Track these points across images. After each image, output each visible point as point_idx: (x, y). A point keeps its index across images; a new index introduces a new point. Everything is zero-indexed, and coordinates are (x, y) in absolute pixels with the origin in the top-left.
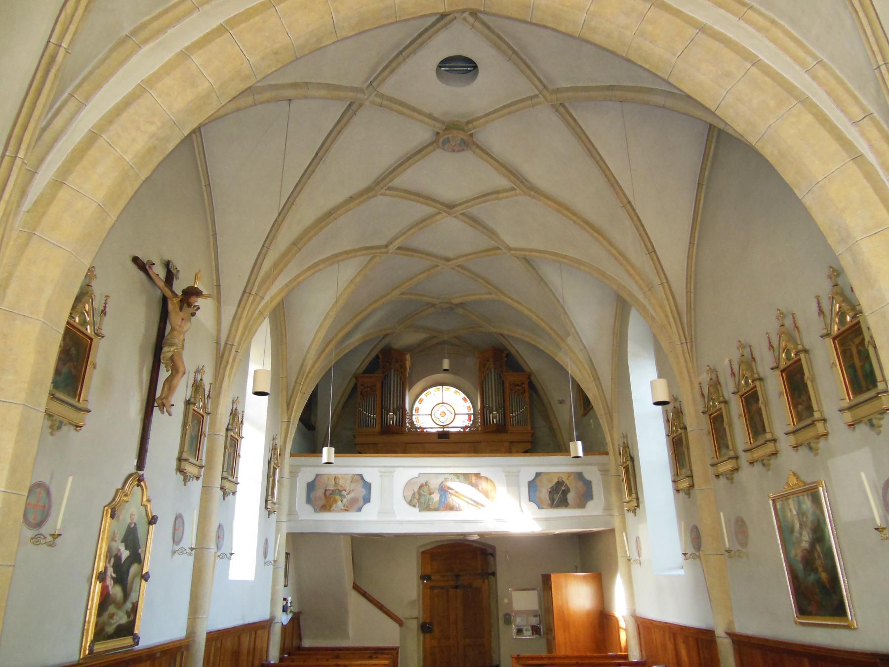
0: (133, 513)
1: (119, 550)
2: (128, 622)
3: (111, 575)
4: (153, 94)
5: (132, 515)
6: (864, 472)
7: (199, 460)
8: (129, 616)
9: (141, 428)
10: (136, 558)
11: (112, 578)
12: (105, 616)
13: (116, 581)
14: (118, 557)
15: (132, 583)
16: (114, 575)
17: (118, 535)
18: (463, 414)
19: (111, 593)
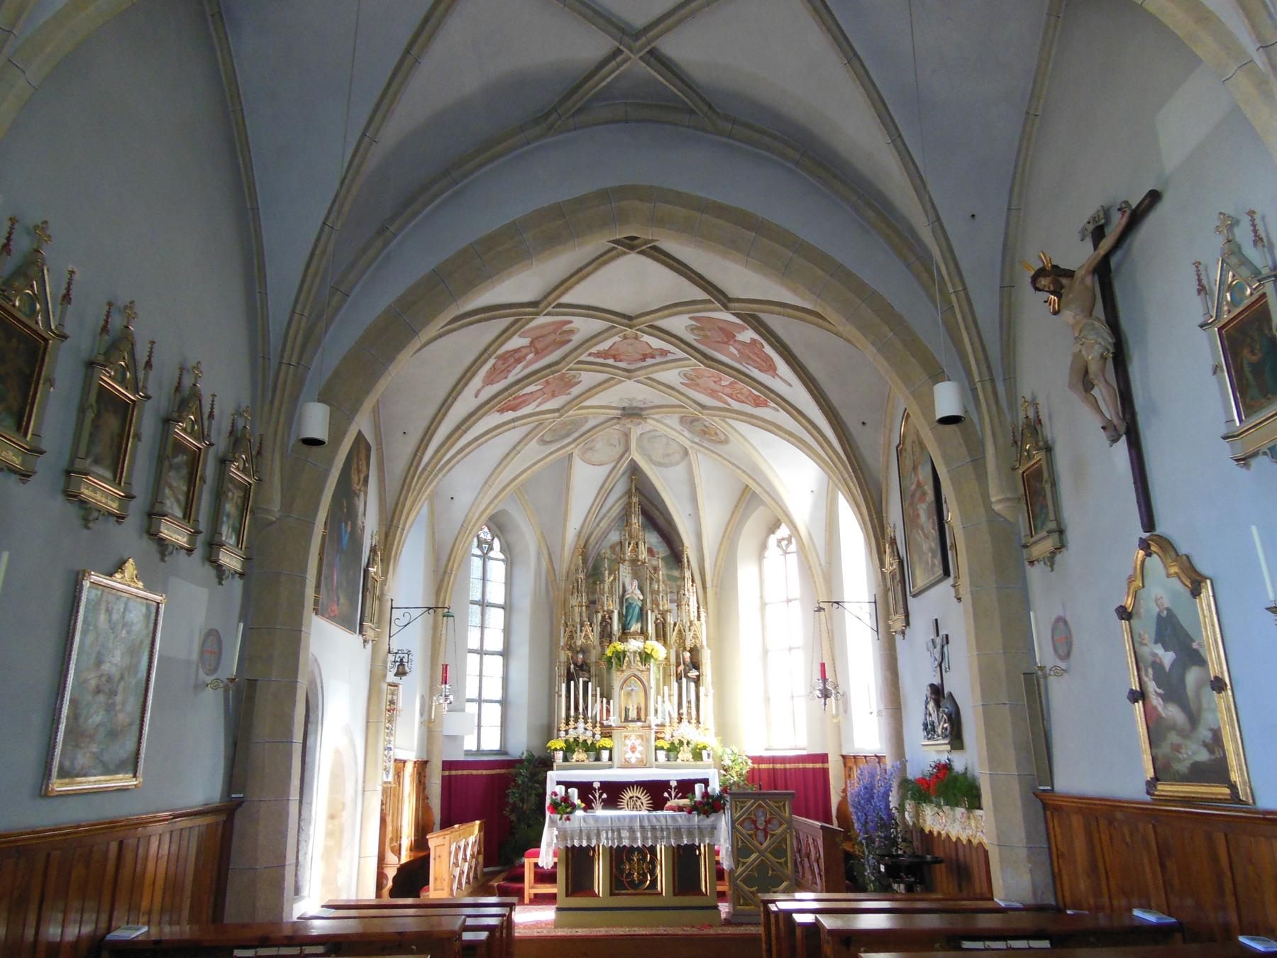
0: (1159, 596)
1: (1155, 655)
2: (1210, 760)
3: (1155, 692)
4: (324, 568)
5: (1157, 600)
6: (1136, 907)
7: (191, 522)
8: (1211, 752)
9: (1135, 478)
10: (1192, 656)
11: (1158, 694)
12: (1165, 749)
13: (1166, 698)
14: (1157, 666)
15: (1199, 701)
16: (1160, 691)
17: (1146, 636)
18: (763, 627)
19: (1164, 715)
